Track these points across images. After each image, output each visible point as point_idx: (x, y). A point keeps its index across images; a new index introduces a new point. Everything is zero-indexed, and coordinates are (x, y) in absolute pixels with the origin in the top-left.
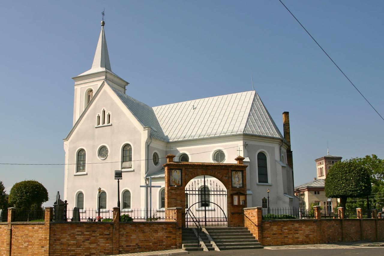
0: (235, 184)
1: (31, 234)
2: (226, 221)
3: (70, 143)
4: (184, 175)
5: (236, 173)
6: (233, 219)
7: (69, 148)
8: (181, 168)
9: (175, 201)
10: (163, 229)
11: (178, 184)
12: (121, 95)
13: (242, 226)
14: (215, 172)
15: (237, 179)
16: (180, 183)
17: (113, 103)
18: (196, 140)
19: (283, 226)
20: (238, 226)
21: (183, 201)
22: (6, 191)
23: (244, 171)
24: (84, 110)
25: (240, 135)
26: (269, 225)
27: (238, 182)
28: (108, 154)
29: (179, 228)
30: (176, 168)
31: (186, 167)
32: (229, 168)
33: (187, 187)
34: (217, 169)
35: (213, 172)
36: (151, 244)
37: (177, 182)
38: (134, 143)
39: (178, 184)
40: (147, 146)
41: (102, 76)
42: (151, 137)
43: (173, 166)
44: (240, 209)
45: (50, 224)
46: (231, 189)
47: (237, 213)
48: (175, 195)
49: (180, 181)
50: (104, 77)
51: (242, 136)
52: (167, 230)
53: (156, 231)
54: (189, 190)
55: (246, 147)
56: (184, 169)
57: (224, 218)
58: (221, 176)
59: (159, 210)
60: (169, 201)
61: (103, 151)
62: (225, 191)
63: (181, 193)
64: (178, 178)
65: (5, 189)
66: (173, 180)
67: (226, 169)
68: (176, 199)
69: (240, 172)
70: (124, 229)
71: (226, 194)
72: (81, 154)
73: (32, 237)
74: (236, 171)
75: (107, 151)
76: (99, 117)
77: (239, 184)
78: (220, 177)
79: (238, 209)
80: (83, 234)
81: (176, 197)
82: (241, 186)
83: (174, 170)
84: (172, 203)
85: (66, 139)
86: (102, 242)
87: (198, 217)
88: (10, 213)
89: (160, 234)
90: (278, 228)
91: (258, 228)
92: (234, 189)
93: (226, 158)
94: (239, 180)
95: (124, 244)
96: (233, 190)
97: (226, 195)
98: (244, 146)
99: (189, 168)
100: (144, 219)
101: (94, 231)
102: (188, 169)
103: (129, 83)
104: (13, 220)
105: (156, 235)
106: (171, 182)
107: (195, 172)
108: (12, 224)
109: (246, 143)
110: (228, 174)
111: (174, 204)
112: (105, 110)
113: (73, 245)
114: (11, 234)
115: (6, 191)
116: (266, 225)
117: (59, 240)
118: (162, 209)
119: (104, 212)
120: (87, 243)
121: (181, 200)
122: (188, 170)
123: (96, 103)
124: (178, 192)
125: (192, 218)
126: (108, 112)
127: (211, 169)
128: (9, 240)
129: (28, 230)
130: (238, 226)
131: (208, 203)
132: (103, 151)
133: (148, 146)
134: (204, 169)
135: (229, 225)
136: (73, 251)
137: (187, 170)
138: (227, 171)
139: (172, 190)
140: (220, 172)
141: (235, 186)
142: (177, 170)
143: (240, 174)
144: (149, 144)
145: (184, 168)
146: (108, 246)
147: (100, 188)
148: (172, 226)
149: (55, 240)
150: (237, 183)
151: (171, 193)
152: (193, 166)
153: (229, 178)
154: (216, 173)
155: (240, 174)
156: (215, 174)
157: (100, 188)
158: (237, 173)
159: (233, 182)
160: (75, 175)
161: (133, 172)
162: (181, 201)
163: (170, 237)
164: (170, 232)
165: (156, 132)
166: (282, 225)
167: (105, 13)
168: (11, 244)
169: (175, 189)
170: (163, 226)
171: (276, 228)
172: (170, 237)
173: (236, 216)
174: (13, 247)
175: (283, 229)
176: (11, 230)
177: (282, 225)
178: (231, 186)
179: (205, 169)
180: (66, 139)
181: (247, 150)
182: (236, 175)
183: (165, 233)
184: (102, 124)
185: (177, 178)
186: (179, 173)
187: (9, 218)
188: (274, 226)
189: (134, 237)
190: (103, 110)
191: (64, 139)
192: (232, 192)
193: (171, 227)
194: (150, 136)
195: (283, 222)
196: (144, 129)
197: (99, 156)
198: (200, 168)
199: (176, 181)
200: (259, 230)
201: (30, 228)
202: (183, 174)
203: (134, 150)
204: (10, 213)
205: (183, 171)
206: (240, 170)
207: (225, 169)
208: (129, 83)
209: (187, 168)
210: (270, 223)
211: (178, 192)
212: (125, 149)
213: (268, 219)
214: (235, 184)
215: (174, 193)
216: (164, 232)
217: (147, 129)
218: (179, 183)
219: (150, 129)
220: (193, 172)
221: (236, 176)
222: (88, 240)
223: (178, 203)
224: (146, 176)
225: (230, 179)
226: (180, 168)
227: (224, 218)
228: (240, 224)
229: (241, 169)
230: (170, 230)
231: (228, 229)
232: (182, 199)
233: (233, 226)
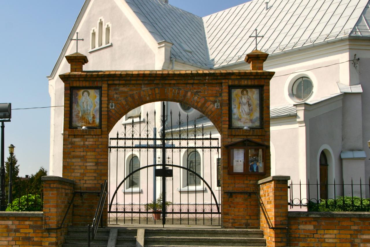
0: (239, 119)
2: (219, 213)
3: (56, 82)
4: (106, 102)
5: (245, 92)
6: (230, 207)
8: (99, 84)
9: (81, 164)
11: (91, 122)
12: (169, 10)
13: (256, 226)
14: (186, 92)
15: (246, 108)
16: (97, 121)
19: (359, 232)
20: (244, 226)
21: (101, 163)
22: (19, 165)
23: (265, 88)
25: (342, 40)
26: (311, 227)
27: (249, 114)
29: (49, 230)
30: (87, 84)
31: (110, 82)
32: (223, 81)
33: (112, 134)
34: (193, 84)
35: (182, 92)
37: (90, 118)
39: (91, 122)
42: (172, 59)
43: (79, 81)
44: (251, 182)
46: (226, 133)
47: (241, 193)
48: (82, 150)
49: (98, 116)
51: (348, 43)
52: (18, 234)
54: (123, 137)
55: (357, 65)
56: (105, 86)
57: (211, 204)
58: (202, 101)
59: (186, 189)
60: (64, 164)
62: (218, 139)
63: (97, 143)
64: (92, 109)
65: (17, 162)
66: (80, 115)
67: (217, 83)
69: (254, 90)
71: (220, 146)
76: (94, 34)
77: (251, 121)
78: (200, 104)
79: (246, 182)
81: (85, 154)
82: (257, 124)
83: (82, 91)
84: (73, 167)
85: (51, 76)
87: (179, 203)
90: (342, 236)
91: (276, 234)
92: (234, 134)
93: (315, 90)
94: (251, 110)
96: (231, 136)
97: (220, 150)
98: (352, 62)
99: (119, 84)
100: (301, 205)
102: (117, 87)
106: (75, 119)
107: (135, 92)
109: (355, 55)
110: (221, 95)
111: (80, 171)
112: (103, 20)
115: (19, 165)
116: (302, 227)
119: (136, 193)
121: (95, 160)
122: (118, 90)
123: (91, 10)
124: (90, 142)
125: (217, 204)
126: (107, 24)
127: (174, 84)
130: (244, 226)
131: (170, 168)
134: (157, 84)
137: (115, 90)
138: (217, 89)
139: (75, 136)
140: (200, 92)
141: (237, 124)
142: (90, 91)
143: (254, 95)
145: (106, 86)
147: (12, 145)
148: (31, 223)
150: (245, 117)
151: (72, 143)
152: (129, 78)
154: (189, 94)
155: (254, 95)
156: (185, 95)
157: (12, 145)
158: (247, 92)
159: (234, 117)
162: (97, 164)
165: (191, 53)
166: (356, 228)
169: (83, 135)
170: (10, 223)
171: (334, 236)
173: (239, 199)
175: (357, 241)
177: (356, 228)
178: (227, 126)
179: (160, 86)
180: (51, 76)
181: (360, 73)
182: (243, 99)
183: (13, 240)
184: (98, 46)
185: (89, 108)
186: (96, 97)
188: (326, 231)
190: (99, 21)
191: (48, 77)
192: (229, 140)
193: (30, 225)
194: (171, 58)
195: (357, 221)
196: (159, 46)
198: (146, 82)
199: (86, 116)
200: (279, 240)
202: (105, 99)
205: (103, 92)
206: (253, 83)
207: (213, 83)
209: (116, 84)
210: (314, 223)
213: (326, 210)
215: (79, 143)
216: (11, 239)
217: (164, 45)
218: (94, 121)
219: (171, 45)
220: (131, 93)
221: (244, 100)
223: (88, 168)
225: (225, 109)
226: (95, 84)
227: (211, 204)
228: (249, 221)
229: (256, 83)
230: (26, 233)
232: (98, 159)
233: (230, 225)
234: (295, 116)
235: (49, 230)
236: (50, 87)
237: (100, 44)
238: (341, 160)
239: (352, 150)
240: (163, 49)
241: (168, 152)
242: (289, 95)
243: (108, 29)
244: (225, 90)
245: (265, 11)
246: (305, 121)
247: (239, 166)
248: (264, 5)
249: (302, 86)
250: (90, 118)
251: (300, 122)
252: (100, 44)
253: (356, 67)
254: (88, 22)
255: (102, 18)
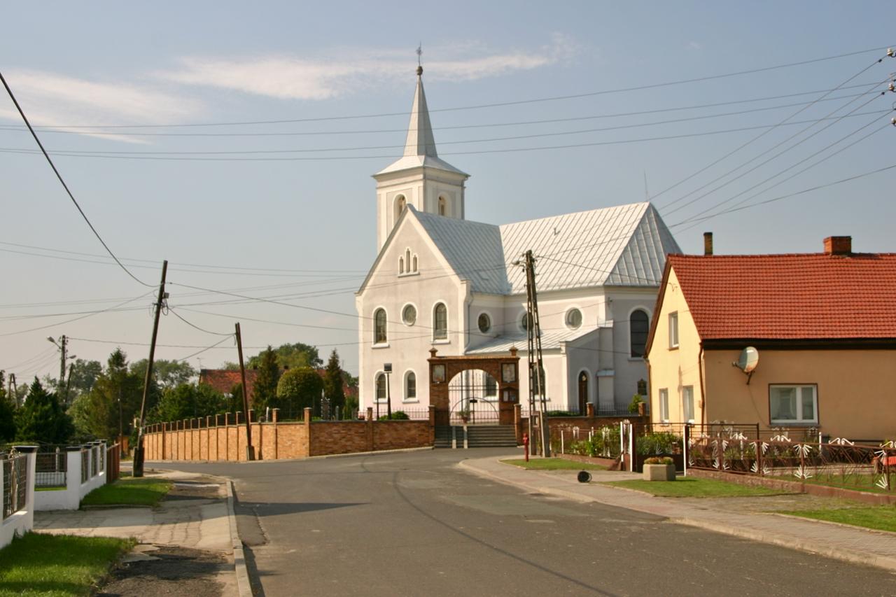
1: (293, 433)
7: (363, 306)
10: (415, 427)
15: (509, 373)
17: (420, 241)
18: (552, 292)
24: (393, 227)
28: (417, 317)
29: (432, 427)
33: (450, 384)
36: (404, 441)
38: (450, 303)
40: (467, 307)
41: (419, 174)
45: (310, 424)
50: (421, 176)
53: (409, 429)
61: (409, 313)
68: (438, 396)
70: (378, 427)
72: (380, 316)
73: (294, 436)
74: (508, 364)
75: (415, 312)
76: (402, 261)
80: (339, 433)
82: (514, 380)
85: (358, 293)
86: (357, 440)
88: (274, 414)
89: (413, 432)
95: (378, 441)
100: (495, 419)
101: (350, 430)
103: (470, 176)
104: (278, 421)
105: (408, 433)
108: (277, 425)
112: (410, 250)
113: (330, 442)
114: (276, 434)
117: (318, 438)
118: (489, 398)
120: (343, 441)
124: (441, 389)
126: (414, 254)
128: (275, 440)
129: (291, 429)
132: (409, 313)
133: (469, 306)
135: (500, 422)
136: (331, 448)
143: (512, 367)
144: (471, 303)
146: (363, 443)
149: (315, 438)
150: (509, 377)
151: (433, 389)
153: (498, 371)
155: (512, 367)
159: (504, 377)
160: (374, 348)
161: (449, 346)
163: (422, 435)
164: (423, 430)
167: (422, 49)
168: (276, 443)
169: (438, 386)
172: (422, 435)
174: (279, 446)
176: (276, 430)
180: (358, 293)
187: (274, 419)
189: (387, 435)
191: (355, 293)
197: (404, 319)
201: (293, 427)
202: (447, 370)
203: (450, 313)
204: (274, 414)
208: (470, 176)
211: (441, 389)
212: (438, 310)
214: (506, 378)
222: (344, 437)
224: (467, 351)
225: (500, 374)
231: (499, 427)
234: (560, 349)
235: (432, 427)
236: (357, 304)
237: (408, 270)
238: (597, 378)
239: (606, 369)
240: (465, 285)
241: (475, 392)
242: (566, 323)
243: (415, 259)
244: (500, 365)
245: (553, 237)
246: (566, 353)
247: (506, 399)
248: (552, 230)
249: (574, 318)
250: (440, 378)
251: (563, 354)
252: (408, 270)
253: (609, 307)
254: (396, 249)
255: (409, 247)
